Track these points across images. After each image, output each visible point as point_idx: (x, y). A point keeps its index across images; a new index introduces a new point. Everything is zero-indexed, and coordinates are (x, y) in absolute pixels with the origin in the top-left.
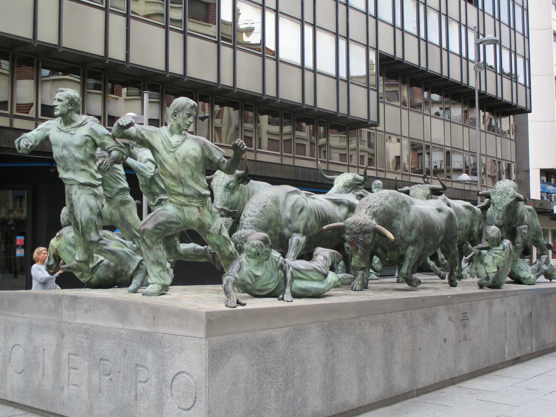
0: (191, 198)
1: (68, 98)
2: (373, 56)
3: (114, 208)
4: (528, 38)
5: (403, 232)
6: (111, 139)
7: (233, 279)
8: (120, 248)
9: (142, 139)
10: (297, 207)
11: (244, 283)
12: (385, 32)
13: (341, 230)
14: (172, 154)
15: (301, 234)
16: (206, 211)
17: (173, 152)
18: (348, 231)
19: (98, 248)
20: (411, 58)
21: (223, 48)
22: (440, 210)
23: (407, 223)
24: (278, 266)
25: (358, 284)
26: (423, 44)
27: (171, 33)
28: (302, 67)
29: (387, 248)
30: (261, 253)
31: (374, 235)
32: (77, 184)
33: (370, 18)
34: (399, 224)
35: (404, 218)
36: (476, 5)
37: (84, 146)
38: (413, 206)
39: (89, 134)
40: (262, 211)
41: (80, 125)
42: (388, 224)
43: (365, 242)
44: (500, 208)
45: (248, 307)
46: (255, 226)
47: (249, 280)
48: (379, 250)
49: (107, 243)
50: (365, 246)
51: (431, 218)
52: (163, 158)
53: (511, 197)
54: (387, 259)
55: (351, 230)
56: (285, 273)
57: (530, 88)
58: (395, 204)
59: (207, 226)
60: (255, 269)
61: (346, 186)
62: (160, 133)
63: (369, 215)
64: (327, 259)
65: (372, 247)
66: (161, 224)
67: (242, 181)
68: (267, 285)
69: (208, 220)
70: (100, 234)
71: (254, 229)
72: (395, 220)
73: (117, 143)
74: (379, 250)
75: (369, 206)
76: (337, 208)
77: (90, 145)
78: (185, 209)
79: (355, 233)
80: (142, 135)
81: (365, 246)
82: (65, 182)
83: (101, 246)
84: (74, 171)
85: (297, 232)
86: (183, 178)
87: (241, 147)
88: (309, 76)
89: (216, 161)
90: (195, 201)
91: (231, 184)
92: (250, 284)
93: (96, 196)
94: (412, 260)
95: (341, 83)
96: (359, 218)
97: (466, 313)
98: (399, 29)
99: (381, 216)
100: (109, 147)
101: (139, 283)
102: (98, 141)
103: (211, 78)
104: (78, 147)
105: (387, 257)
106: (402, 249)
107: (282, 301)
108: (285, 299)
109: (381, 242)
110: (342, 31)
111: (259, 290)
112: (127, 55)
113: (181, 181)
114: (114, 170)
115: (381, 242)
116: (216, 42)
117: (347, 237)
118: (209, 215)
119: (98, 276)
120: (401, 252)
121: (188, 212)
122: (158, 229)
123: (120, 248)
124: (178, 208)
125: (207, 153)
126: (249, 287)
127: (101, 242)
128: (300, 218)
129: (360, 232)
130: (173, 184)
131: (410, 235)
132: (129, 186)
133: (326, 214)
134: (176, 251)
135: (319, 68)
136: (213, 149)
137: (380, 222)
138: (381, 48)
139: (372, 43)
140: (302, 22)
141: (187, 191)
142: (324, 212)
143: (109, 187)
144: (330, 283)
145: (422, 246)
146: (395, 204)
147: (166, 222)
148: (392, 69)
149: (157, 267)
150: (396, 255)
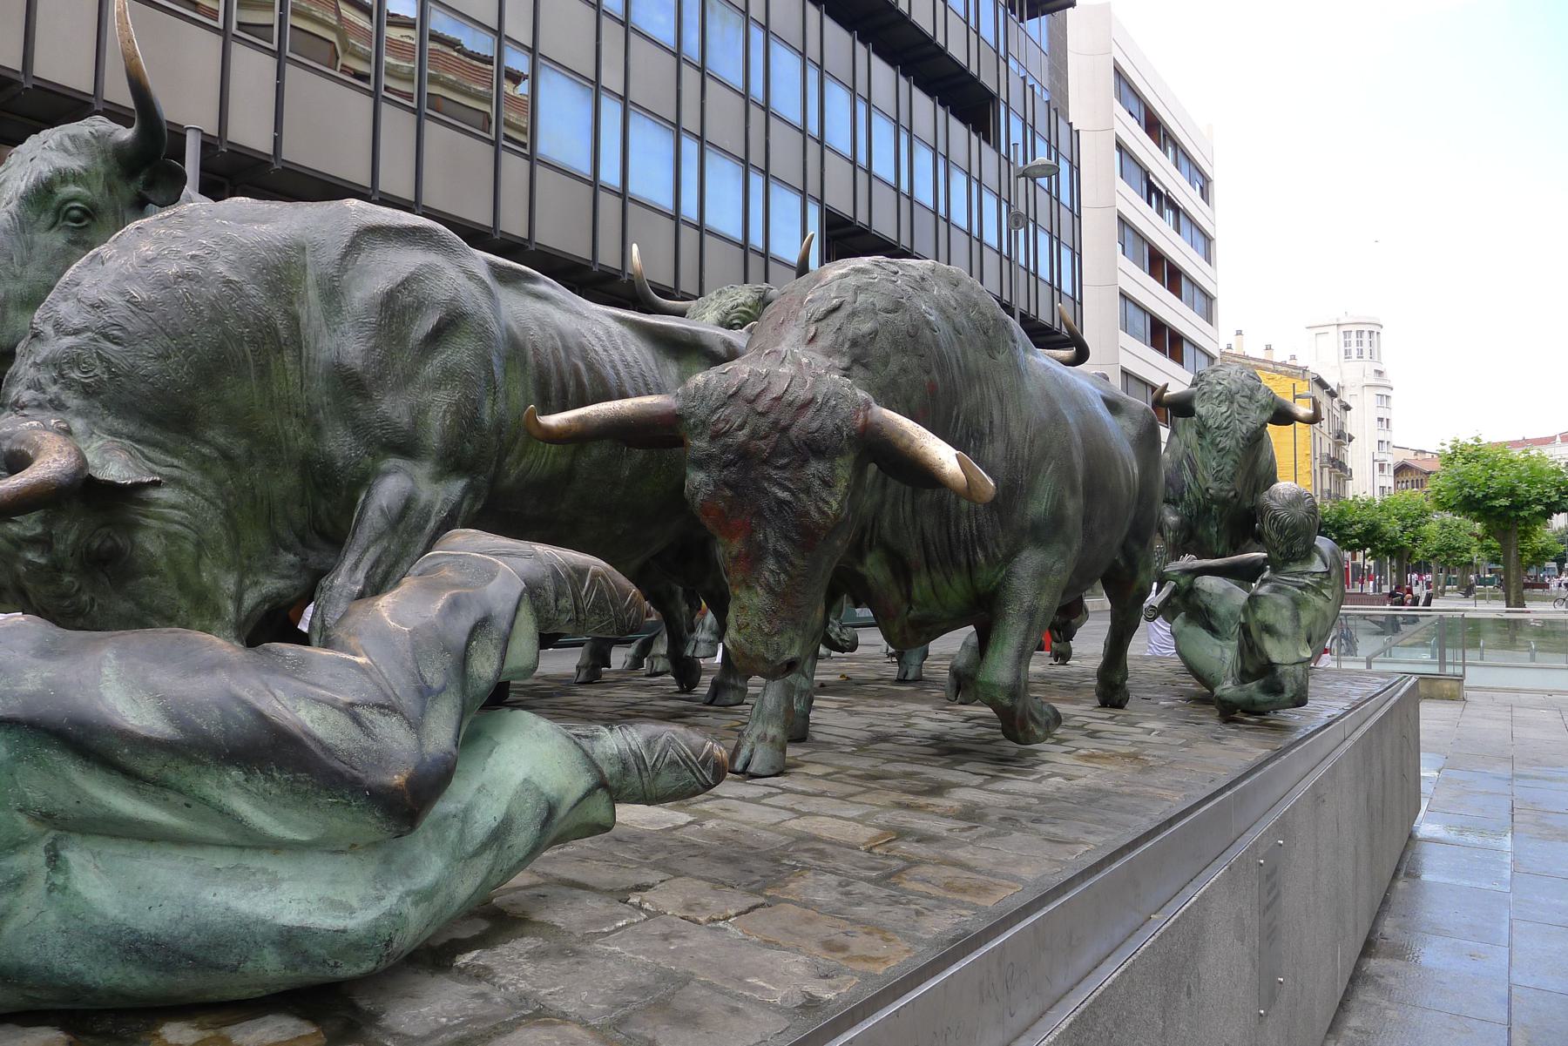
10: (419, 307)
12: (838, 173)
18: (700, 444)
21: (506, 157)
25: (762, 738)
26: (905, 203)
27: (385, 108)
28: (676, 217)
29: (914, 555)
31: (859, 470)
36: (997, 147)
44: (1226, 443)
46: (87, 391)
48: (874, 568)
50: (807, 536)
53: (1264, 408)
57: (1081, 304)
63: (829, 352)
67: (149, 185)
71: (79, 413)
74: (874, 568)
85: (406, 447)
88: (689, 237)
98: (860, 168)
99: (893, 367)
105: (908, 598)
106: (991, 560)
112: (277, 142)
116: (491, 142)
117: (696, 478)
120: (985, 576)
129: (776, 452)
132: (460, 477)
135: (710, 221)
140: (677, 128)
142: (590, 367)
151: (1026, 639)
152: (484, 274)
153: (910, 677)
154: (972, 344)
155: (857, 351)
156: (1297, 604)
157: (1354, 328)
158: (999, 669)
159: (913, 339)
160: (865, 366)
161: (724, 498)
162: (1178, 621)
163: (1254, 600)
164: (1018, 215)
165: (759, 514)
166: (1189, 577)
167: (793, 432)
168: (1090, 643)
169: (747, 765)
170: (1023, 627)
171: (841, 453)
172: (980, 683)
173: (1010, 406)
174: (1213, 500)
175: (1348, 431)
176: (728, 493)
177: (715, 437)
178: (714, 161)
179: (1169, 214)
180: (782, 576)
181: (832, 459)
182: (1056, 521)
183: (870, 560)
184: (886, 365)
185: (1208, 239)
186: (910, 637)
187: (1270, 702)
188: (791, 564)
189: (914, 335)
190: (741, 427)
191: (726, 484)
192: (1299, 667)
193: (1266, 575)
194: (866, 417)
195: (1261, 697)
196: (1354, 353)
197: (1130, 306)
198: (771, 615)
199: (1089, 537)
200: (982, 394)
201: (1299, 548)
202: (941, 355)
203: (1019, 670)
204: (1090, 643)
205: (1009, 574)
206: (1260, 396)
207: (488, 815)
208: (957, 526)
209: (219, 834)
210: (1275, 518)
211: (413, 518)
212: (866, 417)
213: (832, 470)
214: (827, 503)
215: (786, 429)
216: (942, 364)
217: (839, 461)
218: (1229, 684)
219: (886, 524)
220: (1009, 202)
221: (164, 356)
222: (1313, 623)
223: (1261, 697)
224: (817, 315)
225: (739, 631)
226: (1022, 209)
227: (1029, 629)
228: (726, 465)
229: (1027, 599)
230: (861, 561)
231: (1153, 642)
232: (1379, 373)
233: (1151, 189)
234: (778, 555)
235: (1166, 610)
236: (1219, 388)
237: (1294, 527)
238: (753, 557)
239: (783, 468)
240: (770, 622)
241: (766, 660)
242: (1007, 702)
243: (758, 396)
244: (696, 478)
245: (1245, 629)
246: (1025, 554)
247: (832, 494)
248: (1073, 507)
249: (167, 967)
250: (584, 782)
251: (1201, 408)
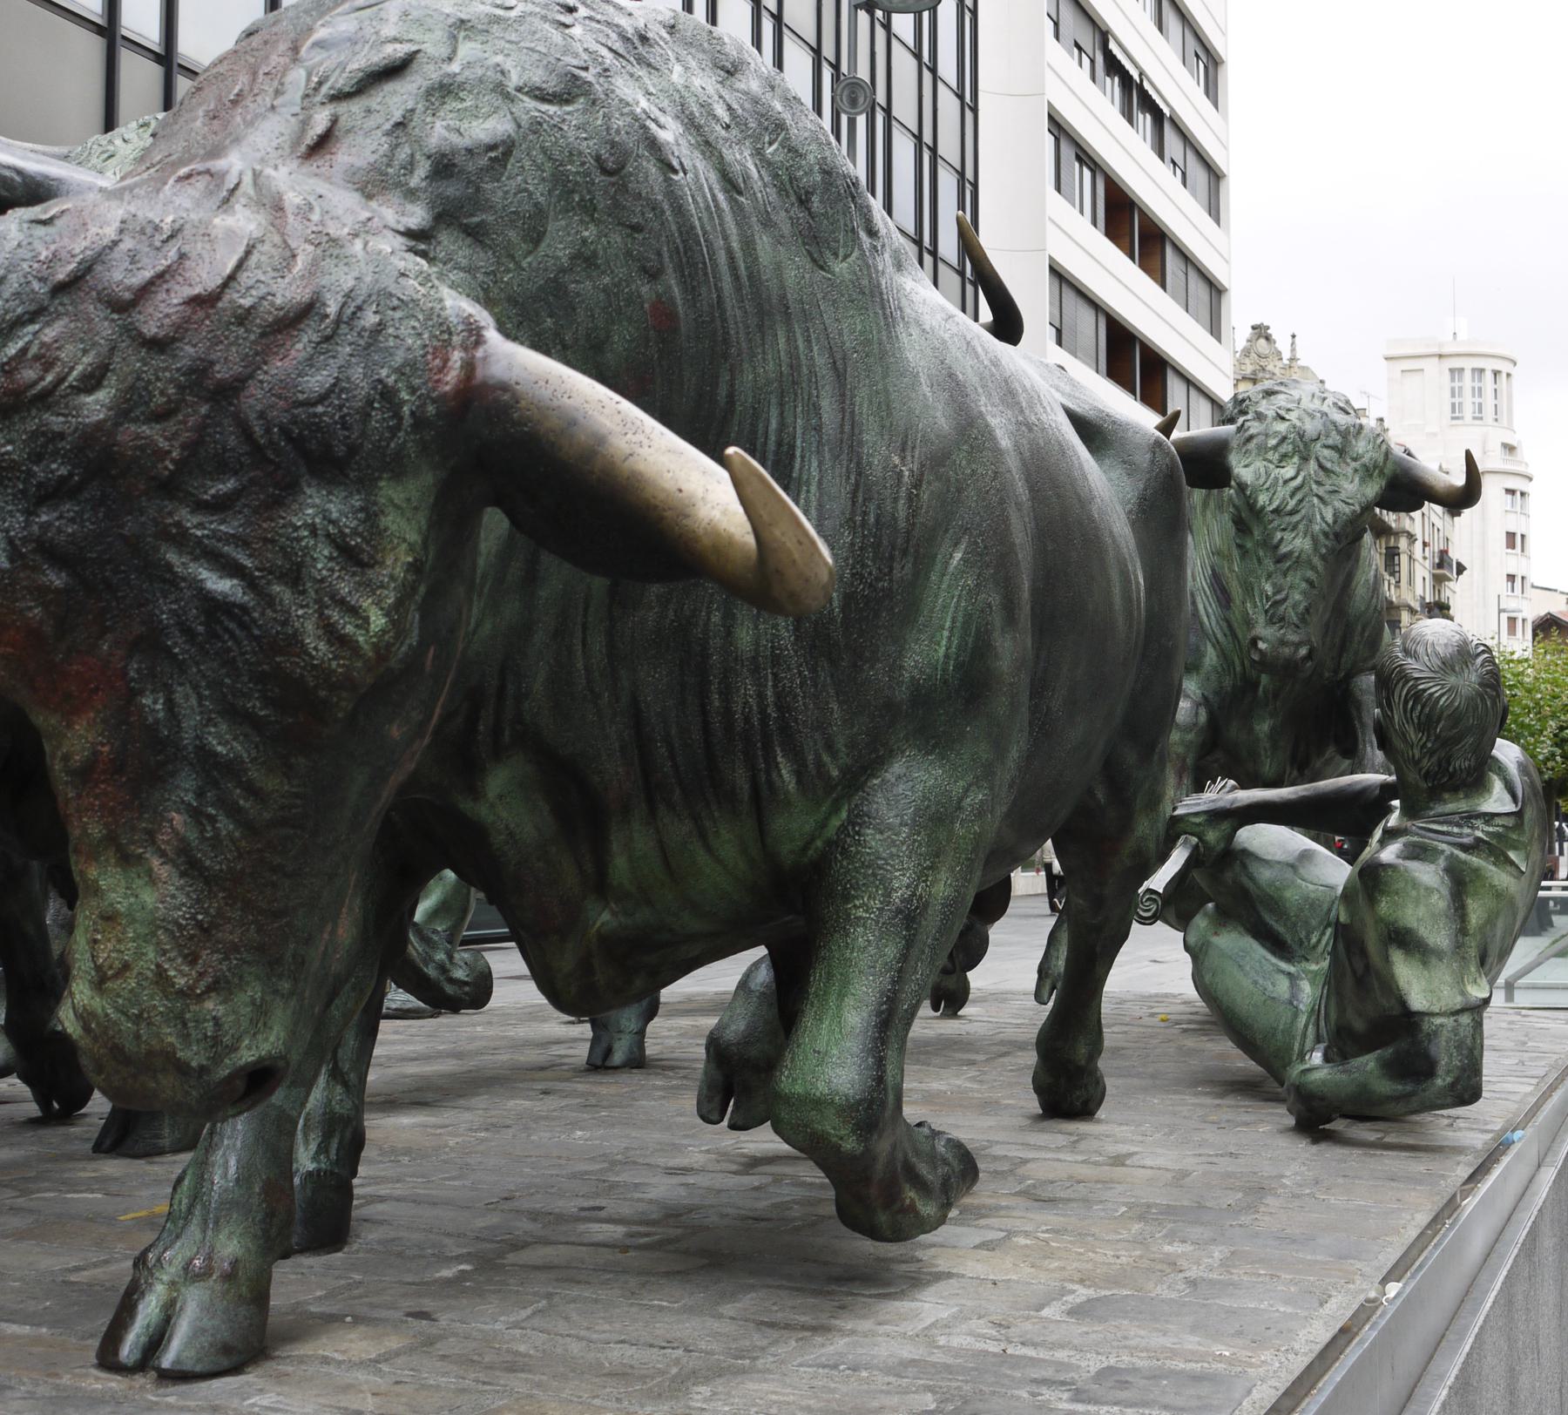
4: (975, 110)
31: (451, 524)
44: (1297, 543)
48: (505, 803)
50: (298, 709)
53: (1368, 472)
54: (604, 918)
63: (372, 184)
65: (406, 741)
74: (505, 803)
99: (560, 242)
105: (600, 886)
109: (538, 684)
120: (795, 827)
151: (899, 978)
153: (618, 1057)
154: (767, 223)
155: (452, 189)
156: (1460, 882)
157: (1468, 364)
158: (832, 1060)
159: (611, 181)
160: (476, 234)
161: (42, 593)
162: (1200, 922)
163: (1372, 879)
164: (855, 85)
165: (150, 643)
166: (1226, 826)
167: (254, 398)
168: (1013, 964)
169: (156, 1341)
170: (891, 952)
171: (397, 467)
172: (787, 1099)
173: (862, 394)
174: (1265, 663)
175: (1455, 555)
176: (56, 579)
179: (1145, 120)
180: (225, 825)
181: (366, 484)
182: (971, 681)
183: (497, 781)
184: (535, 237)
185: (1215, 175)
186: (607, 981)
187: (1405, 1097)
188: (252, 790)
190: (92, 382)
191: (50, 552)
192: (1465, 1019)
193: (1393, 820)
194: (469, 367)
195: (1385, 1087)
196: (1468, 411)
197: (1069, 296)
198: (193, 939)
199: (1043, 729)
200: (793, 354)
201: (1461, 763)
202: (687, 231)
203: (880, 1063)
204: (1013, 964)
205: (857, 820)
206: (1361, 446)
208: (727, 693)
210: (1417, 696)
212: (469, 367)
213: (370, 515)
214: (354, 611)
215: (227, 392)
216: (689, 254)
217: (390, 492)
218: (1317, 1058)
219: (538, 684)
220: (836, 67)
222: (1490, 921)
223: (1385, 1087)
224: (340, 81)
225: (100, 982)
226: (863, 73)
227: (904, 957)
228: (51, 494)
229: (901, 883)
231: (1152, 968)
232: (1510, 448)
233: (1114, 66)
234: (210, 765)
235: (1177, 906)
236: (1281, 427)
237: (1456, 717)
238: (143, 763)
239: (220, 506)
240: (192, 959)
241: (182, 1068)
242: (850, 1145)
243: (145, 291)
245: (1348, 941)
246: (897, 767)
247: (369, 587)
248: (1010, 650)
251: (1245, 469)
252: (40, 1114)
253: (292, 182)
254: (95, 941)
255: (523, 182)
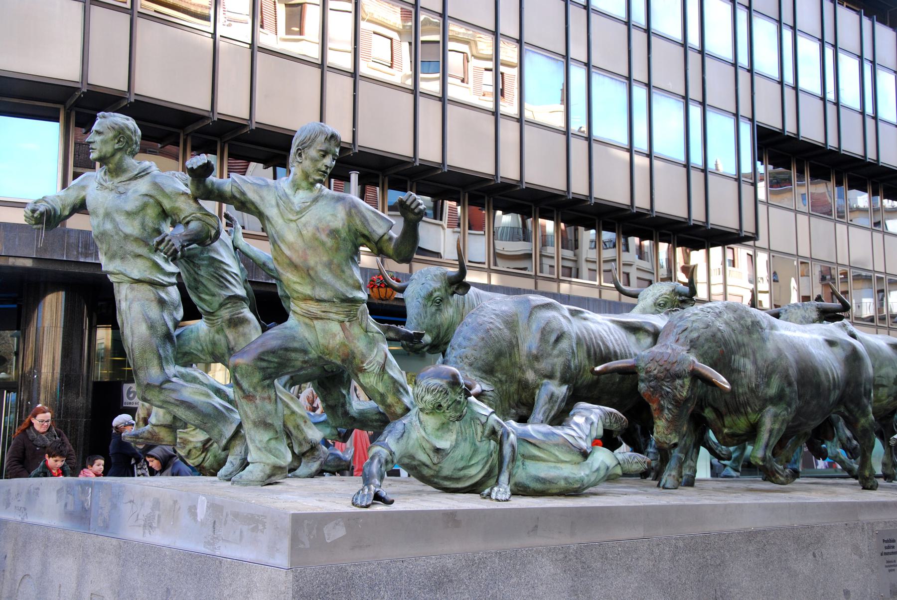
0: (327, 304)
1: (113, 128)
2: (746, 130)
3: (218, 333)
5: (753, 380)
6: (191, 202)
7: (384, 453)
8: (203, 399)
9: (242, 198)
11: (415, 463)
12: (767, 95)
13: (630, 373)
14: (293, 225)
15: (556, 382)
16: (356, 330)
17: (295, 221)
19: (162, 397)
20: (811, 132)
22: (831, 343)
23: (760, 363)
24: (487, 432)
29: (723, 409)
30: (445, 405)
32: (129, 282)
33: (690, 53)
34: (747, 365)
35: (754, 353)
37: (141, 214)
38: (775, 332)
39: (150, 193)
40: (483, 339)
41: (136, 177)
42: (723, 363)
43: (675, 396)
45: (396, 507)
46: (471, 365)
47: (423, 457)
49: (178, 387)
51: (810, 354)
52: (277, 232)
54: (726, 431)
55: (647, 372)
56: (501, 444)
58: (736, 325)
59: (359, 356)
60: (437, 437)
61: (659, 305)
62: (276, 188)
64: (592, 424)
65: (691, 406)
66: (273, 352)
67: (457, 289)
68: (463, 468)
69: (360, 345)
70: (167, 371)
72: (737, 357)
73: (201, 208)
74: (708, 414)
75: (683, 328)
76: (632, 338)
77: (152, 212)
78: (318, 324)
79: (656, 378)
80: (243, 194)
81: (679, 404)
82: (112, 278)
83: (166, 393)
84: (123, 258)
85: (550, 376)
86: (313, 269)
87: (413, 206)
89: (376, 238)
90: (334, 310)
91: (435, 295)
92: (427, 466)
93: (162, 303)
94: (775, 433)
95: (693, 173)
96: (663, 350)
97: (894, 541)
99: (706, 347)
100: (187, 214)
101: (237, 462)
102: (167, 205)
103: (485, 167)
104: (129, 214)
105: (724, 426)
107: (488, 501)
108: (493, 496)
110: (695, 93)
111: (447, 478)
113: (308, 273)
114: (216, 264)
115: (710, 397)
118: (362, 336)
119: (215, 456)
120: (753, 417)
121: (324, 330)
122: (264, 360)
123: (203, 399)
124: (306, 324)
125: (358, 222)
126: (426, 472)
127: (166, 386)
128: (556, 352)
129: (666, 377)
130: (295, 279)
131: (768, 385)
133: (607, 347)
134: (346, 413)
136: (370, 216)
137: (704, 358)
138: (761, 118)
139: (745, 110)
141: (321, 293)
143: (207, 294)
144: (598, 470)
145: (794, 407)
146: (736, 325)
147: (281, 349)
148: (781, 151)
149: (262, 432)
150: (742, 424)
152: (567, 314)
154: (740, 333)
171: (686, 377)
177: (647, 372)
178: (659, 101)
189: (714, 336)
207: (596, 466)
209: (552, 459)
211: (554, 399)
215: (668, 370)
221: (487, 353)
230: (703, 410)
238: (661, 409)
244: (642, 386)
249: (544, 483)
250: (615, 463)
252: (62, 295)
253: (675, 346)
254: (652, 554)
255: (702, 340)
